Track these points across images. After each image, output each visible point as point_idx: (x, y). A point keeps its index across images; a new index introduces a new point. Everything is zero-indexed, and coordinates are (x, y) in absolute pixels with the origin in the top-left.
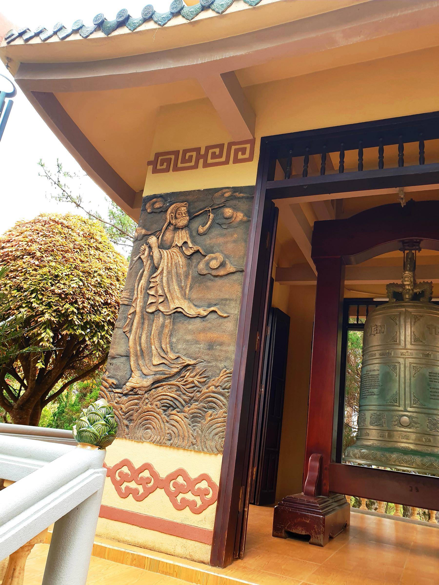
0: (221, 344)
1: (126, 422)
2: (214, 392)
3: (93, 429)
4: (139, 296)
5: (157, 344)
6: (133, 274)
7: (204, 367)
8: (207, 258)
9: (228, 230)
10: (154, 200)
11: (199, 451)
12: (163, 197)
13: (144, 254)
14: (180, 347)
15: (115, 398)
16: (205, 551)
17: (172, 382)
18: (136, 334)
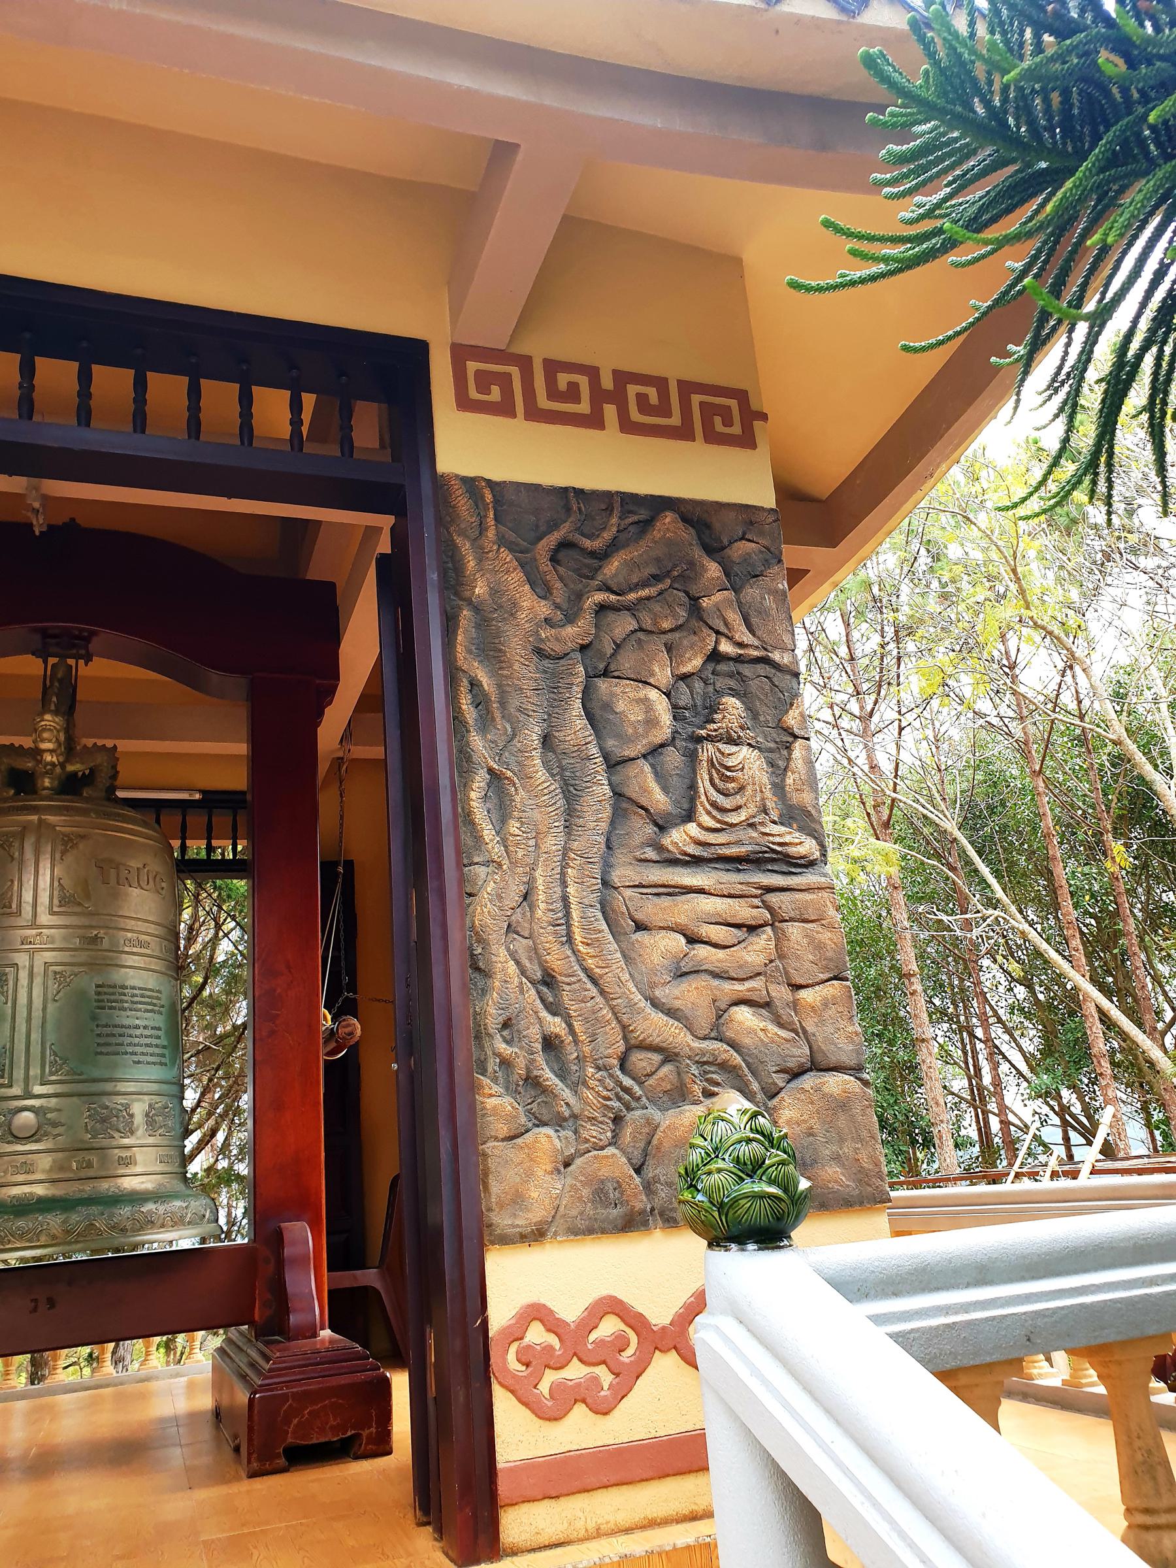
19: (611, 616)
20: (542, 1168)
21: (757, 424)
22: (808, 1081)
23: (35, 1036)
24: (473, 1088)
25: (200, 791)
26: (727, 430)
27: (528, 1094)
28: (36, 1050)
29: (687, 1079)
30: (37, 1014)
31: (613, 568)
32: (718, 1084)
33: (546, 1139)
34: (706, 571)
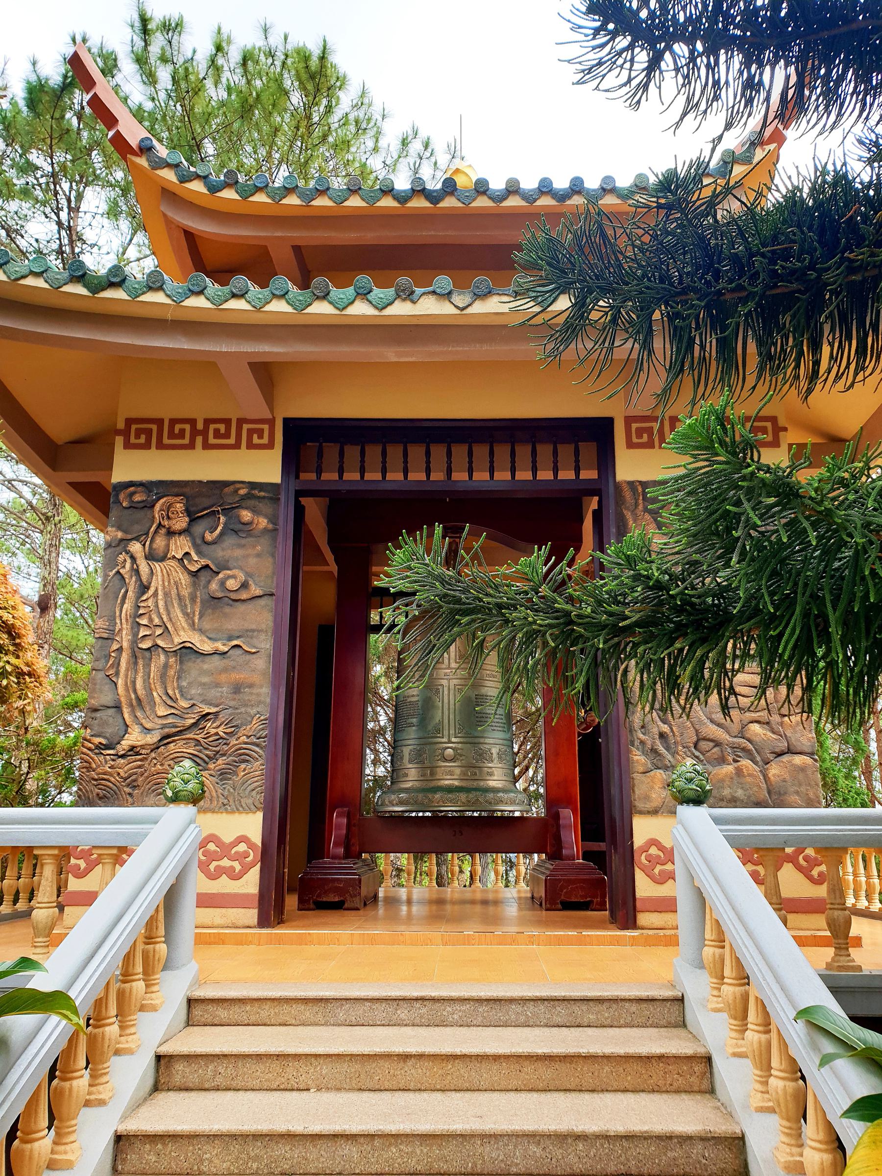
0: (251, 686)
1: (128, 790)
2: (246, 743)
4: (124, 626)
5: (161, 691)
7: (230, 715)
8: (221, 576)
9: (247, 539)
10: (132, 489)
11: (233, 812)
12: (147, 486)
13: (124, 567)
14: (193, 692)
15: (106, 762)
16: (251, 915)
17: (187, 736)
20: (658, 786)
21: (781, 434)
22: (785, 758)
23: (452, 717)
24: (629, 751)
26: (137, 441)
27: (652, 756)
28: (452, 722)
29: (725, 753)
30: (452, 706)
32: (740, 757)
33: (659, 774)
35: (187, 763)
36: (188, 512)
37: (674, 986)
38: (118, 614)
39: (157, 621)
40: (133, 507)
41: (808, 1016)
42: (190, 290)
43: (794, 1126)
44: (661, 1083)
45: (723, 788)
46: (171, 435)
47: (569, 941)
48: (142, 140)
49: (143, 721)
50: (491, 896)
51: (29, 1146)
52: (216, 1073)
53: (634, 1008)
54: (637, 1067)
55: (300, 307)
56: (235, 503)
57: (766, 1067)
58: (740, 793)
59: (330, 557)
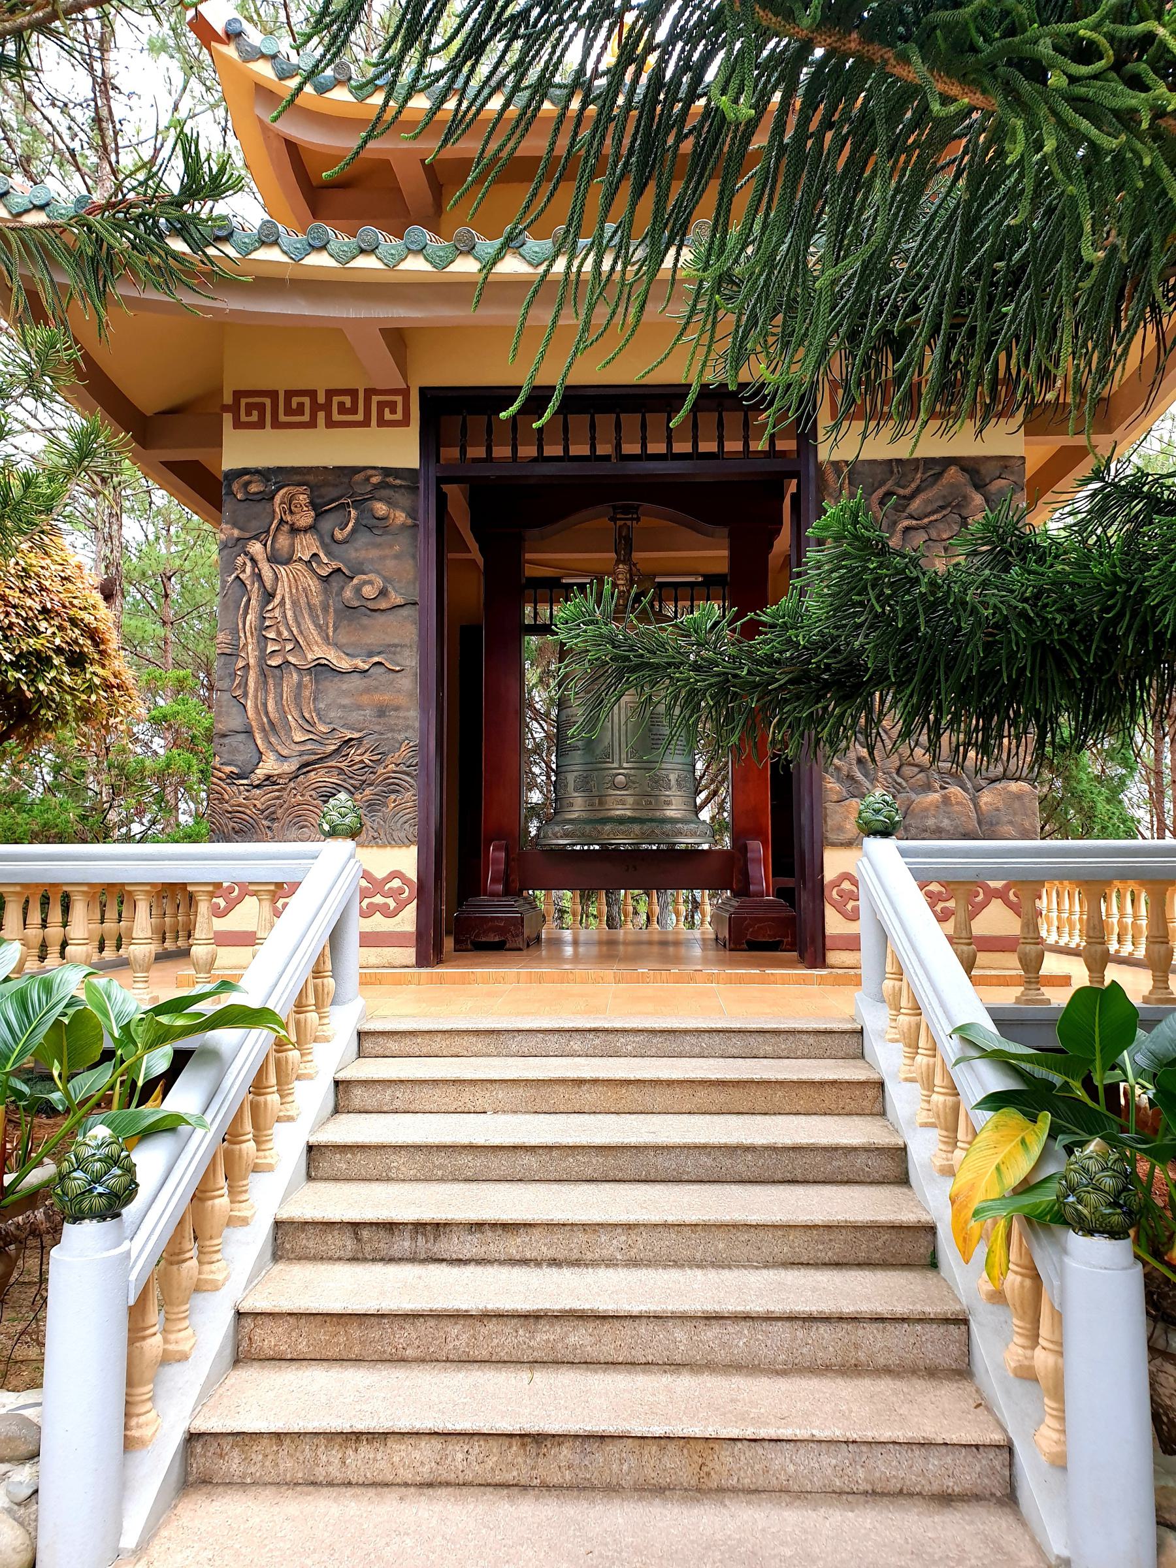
0: (397, 709)
1: (265, 823)
2: (395, 772)
3: (347, 821)
4: (250, 640)
5: (296, 714)
6: (232, 605)
7: (376, 740)
8: (355, 581)
9: (384, 538)
10: (246, 477)
11: (384, 846)
12: (264, 474)
13: (244, 571)
14: (332, 715)
15: (240, 793)
16: (409, 954)
17: (329, 764)
18: (256, 698)
19: (913, 533)
22: (998, 785)
24: (822, 779)
25: (702, 575)
29: (932, 780)
31: (915, 505)
34: (973, 500)
35: (343, 796)
36: (313, 505)
37: (854, 1020)
38: (241, 626)
39: (286, 634)
40: (249, 499)
41: (964, 1033)
42: (310, 245)
43: (951, 1135)
44: (833, 1106)
45: (927, 817)
46: (289, 411)
47: (752, 980)
48: (229, 23)
49: (279, 748)
50: (671, 938)
51: (238, 1147)
52: (394, 1098)
53: (811, 1040)
54: (811, 1092)
55: (442, 263)
56: (367, 494)
57: (930, 1086)
58: (945, 823)
59: (473, 545)
